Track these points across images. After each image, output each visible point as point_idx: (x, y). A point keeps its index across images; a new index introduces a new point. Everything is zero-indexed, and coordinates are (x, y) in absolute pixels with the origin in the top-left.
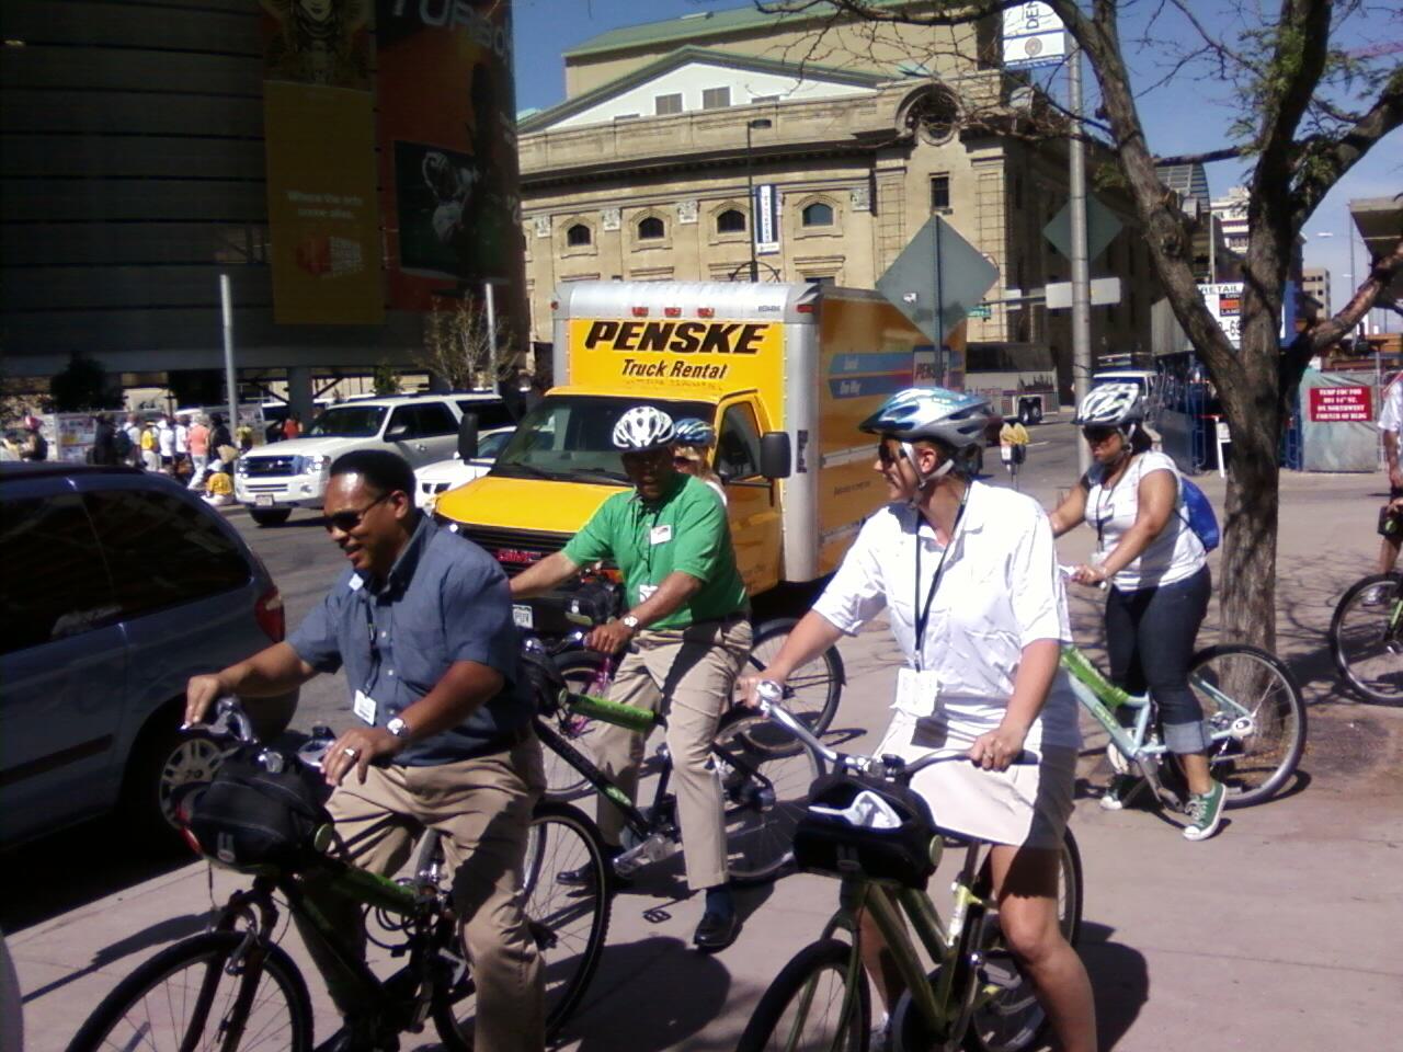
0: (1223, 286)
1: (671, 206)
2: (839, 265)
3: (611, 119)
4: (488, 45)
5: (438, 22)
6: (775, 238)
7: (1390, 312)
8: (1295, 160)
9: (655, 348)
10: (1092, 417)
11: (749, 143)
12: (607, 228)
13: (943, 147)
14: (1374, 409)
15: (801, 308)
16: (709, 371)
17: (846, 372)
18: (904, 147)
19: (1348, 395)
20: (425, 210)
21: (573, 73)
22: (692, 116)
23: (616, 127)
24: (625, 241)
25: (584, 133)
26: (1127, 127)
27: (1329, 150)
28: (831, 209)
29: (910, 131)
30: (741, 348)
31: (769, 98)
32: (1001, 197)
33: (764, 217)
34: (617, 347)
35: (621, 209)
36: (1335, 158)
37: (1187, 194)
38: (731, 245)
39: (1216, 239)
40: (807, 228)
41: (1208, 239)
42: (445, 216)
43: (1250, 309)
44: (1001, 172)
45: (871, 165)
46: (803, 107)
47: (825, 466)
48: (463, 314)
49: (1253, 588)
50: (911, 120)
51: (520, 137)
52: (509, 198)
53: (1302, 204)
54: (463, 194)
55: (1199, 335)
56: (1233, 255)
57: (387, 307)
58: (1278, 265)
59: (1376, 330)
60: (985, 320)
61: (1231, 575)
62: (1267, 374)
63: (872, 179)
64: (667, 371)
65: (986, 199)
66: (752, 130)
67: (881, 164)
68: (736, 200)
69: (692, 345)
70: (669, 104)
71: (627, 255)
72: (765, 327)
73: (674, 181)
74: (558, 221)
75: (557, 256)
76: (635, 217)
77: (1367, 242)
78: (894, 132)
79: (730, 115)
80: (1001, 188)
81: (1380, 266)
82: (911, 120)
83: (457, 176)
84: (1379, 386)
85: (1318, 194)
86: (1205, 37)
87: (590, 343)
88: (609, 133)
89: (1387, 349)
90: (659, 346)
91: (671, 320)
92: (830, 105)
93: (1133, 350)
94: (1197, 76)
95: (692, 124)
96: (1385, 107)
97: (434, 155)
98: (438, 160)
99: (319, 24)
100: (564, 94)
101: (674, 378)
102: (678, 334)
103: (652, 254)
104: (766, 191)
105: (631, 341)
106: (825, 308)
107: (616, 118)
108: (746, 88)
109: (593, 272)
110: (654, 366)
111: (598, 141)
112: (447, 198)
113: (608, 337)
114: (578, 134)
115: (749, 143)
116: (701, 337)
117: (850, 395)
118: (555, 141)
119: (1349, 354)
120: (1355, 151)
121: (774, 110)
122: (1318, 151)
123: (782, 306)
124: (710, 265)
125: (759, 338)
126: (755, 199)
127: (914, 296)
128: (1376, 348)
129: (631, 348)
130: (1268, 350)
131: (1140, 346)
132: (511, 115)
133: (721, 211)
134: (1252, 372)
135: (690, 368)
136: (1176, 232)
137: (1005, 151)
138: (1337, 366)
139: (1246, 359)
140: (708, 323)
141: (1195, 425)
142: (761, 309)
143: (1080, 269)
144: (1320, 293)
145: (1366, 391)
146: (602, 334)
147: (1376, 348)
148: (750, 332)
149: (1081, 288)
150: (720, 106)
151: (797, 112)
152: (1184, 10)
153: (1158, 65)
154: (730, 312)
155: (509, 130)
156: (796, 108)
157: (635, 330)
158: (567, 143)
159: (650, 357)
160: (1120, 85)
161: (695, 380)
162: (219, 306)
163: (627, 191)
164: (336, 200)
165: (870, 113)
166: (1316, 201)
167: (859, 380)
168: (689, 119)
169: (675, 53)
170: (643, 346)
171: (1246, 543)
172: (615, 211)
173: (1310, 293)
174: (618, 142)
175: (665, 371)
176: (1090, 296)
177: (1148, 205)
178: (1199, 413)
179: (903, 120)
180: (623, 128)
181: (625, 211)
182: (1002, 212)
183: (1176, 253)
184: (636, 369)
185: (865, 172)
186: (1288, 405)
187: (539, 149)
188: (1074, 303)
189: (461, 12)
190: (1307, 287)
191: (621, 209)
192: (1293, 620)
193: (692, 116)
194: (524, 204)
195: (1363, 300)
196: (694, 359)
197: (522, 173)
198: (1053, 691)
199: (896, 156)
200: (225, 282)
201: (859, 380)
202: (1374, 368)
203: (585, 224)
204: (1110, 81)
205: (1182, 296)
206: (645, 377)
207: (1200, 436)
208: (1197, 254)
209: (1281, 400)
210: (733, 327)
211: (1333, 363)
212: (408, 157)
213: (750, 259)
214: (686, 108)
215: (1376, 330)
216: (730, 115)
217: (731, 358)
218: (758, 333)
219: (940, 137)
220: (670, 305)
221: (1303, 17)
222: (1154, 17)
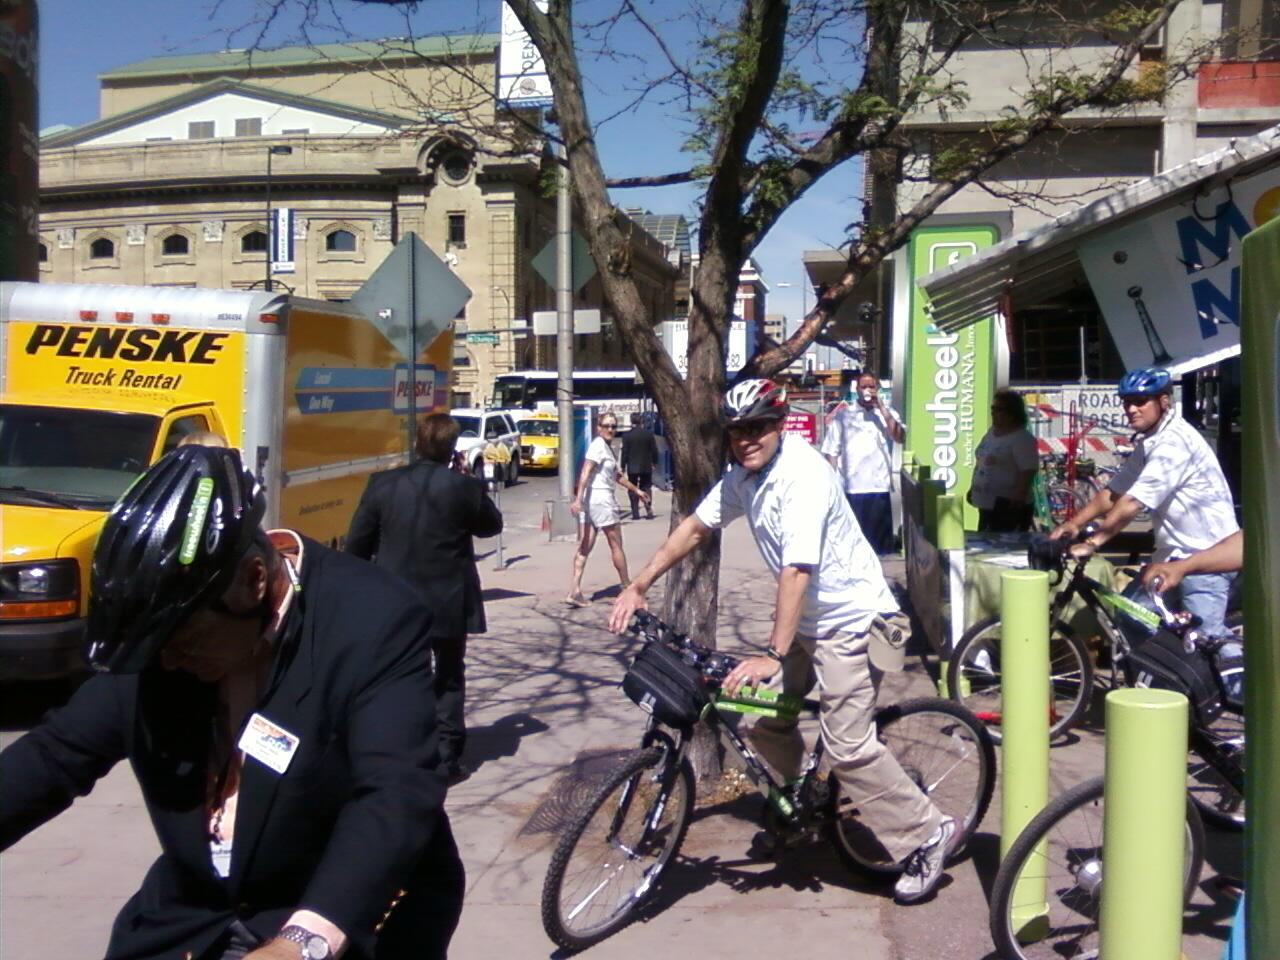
1: (50, 233)
4: (10, 55)
6: (291, 258)
7: (834, 350)
8: (748, 180)
9: (104, 355)
11: (269, 170)
12: (131, 243)
13: (460, 188)
14: (818, 434)
15: (265, 318)
16: (162, 381)
17: (319, 386)
18: (426, 184)
19: (797, 422)
21: (107, 94)
23: (145, 148)
25: (113, 152)
26: (577, 132)
27: (782, 174)
29: (430, 171)
30: (198, 357)
31: (299, 131)
32: (512, 237)
33: (280, 242)
34: (60, 353)
35: (147, 225)
36: (787, 182)
37: (672, 246)
38: (255, 264)
43: (697, 334)
44: (512, 215)
45: (393, 198)
46: (331, 142)
47: (289, 485)
49: (694, 623)
50: (431, 160)
52: (24, 208)
53: (751, 228)
55: (644, 359)
58: (726, 289)
59: (822, 367)
60: (495, 345)
61: (673, 609)
63: (394, 213)
64: (115, 381)
65: (498, 238)
66: (273, 156)
67: (402, 199)
68: (107, 229)
70: (202, 130)
72: (225, 336)
74: (154, 230)
75: (78, 268)
78: (415, 170)
80: (512, 228)
81: (826, 296)
82: (431, 160)
84: (823, 414)
85: (770, 218)
86: (672, 63)
87: (32, 348)
90: (108, 353)
94: (661, 100)
95: (222, 149)
96: (837, 134)
100: (98, 113)
101: (124, 387)
102: (129, 341)
103: (175, 268)
105: (77, 347)
106: (298, 326)
107: (149, 140)
108: (278, 120)
110: (102, 375)
111: (128, 160)
113: (52, 342)
114: (107, 153)
115: (269, 170)
116: (155, 344)
118: (84, 157)
119: (799, 387)
121: (302, 142)
122: (773, 175)
123: (244, 315)
124: (233, 283)
125: (218, 348)
126: (272, 223)
127: (389, 312)
128: (820, 382)
129: (77, 354)
130: (715, 376)
132: (34, 126)
133: (248, 231)
135: (142, 377)
136: (623, 248)
137: (516, 196)
139: (693, 385)
140: (162, 330)
142: (221, 317)
143: (564, 299)
144: (778, 335)
145: (812, 418)
148: (208, 342)
149: (565, 317)
150: (252, 134)
152: (654, 34)
153: (626, 89)
154: (186, 319)
155: (30, 142)
157: (82, 335)
158: (96, 160)
159: (98, 364)
160: (572, 86)
161: (146, 389)
163: (153, 209)
165: (394, 152)
167: (331, 395)
168: (220, 145)
169: (209, 84)
170: (90, 353)
171: (687, 576)
173: (769, 335)
175: (113, 380)
176: (573, 325)
180: (155, 149)
181: (150, 227)
182: (512, 250)
183: (622, 271)
184: (81, 377)
185: (388, 205)
187: (67, 165)
190: (767, 330)
192: (740, 637)
193: (223, 142)
194: (43, 217)
196: (147, 367)
199: (417, 193)
201: (331, 395)
204: (561, 81)
205: (628, 316)
206: (91, 386)
208: (679, 298)
210: (190, 336)
213: (264, 278)
214: (218, 134)
215: (822, 367)
217: (187, 369)
218: (216, 342)
219: (457, 179)
220: (122, 310)
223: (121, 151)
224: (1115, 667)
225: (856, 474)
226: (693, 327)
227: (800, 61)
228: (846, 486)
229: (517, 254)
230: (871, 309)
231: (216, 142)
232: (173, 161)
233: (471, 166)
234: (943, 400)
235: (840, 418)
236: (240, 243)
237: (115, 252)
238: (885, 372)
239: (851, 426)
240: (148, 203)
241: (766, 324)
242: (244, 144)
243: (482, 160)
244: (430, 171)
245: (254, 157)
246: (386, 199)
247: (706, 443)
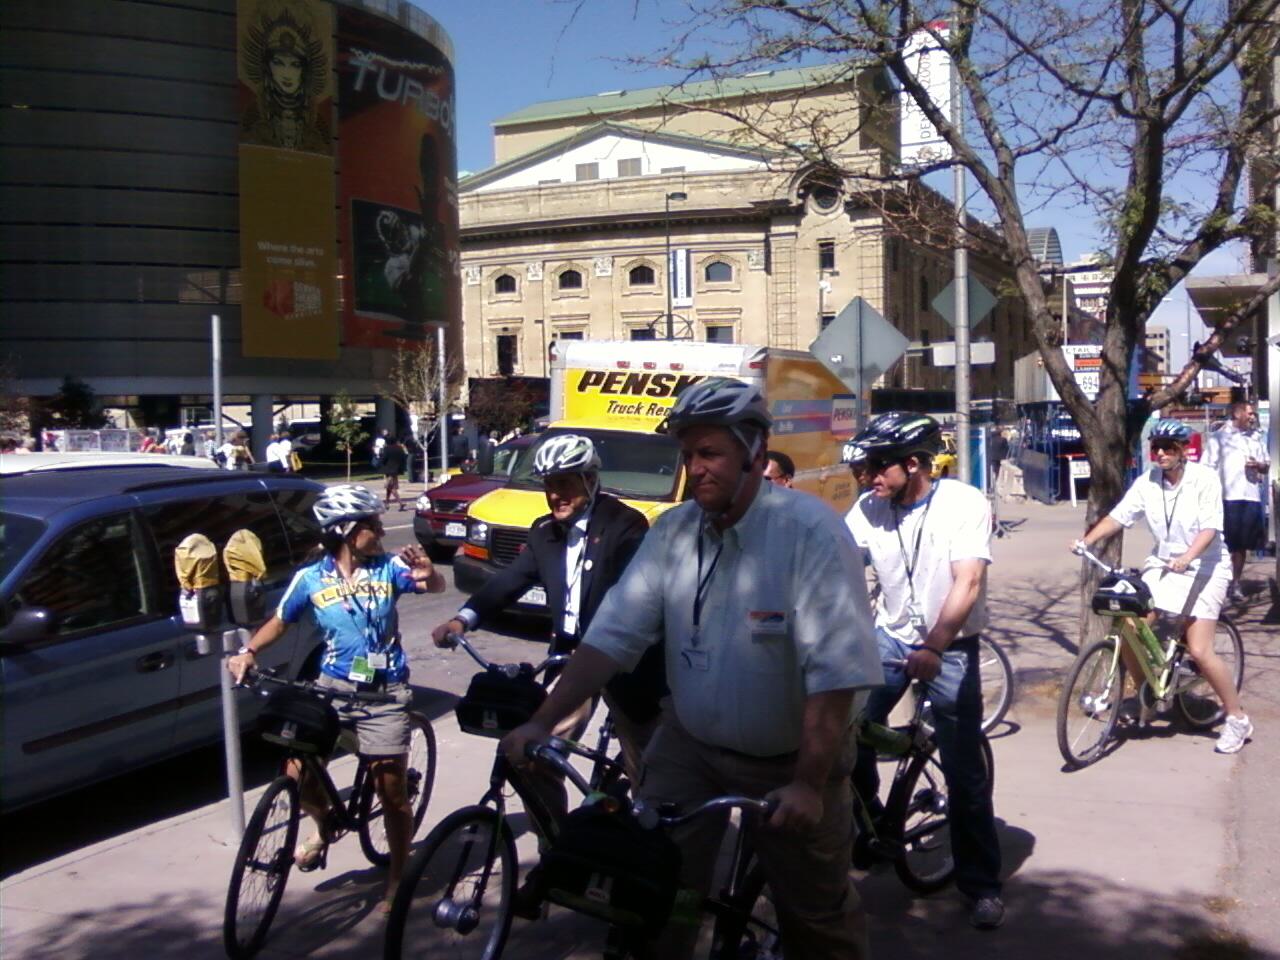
0: (1077, 347)
1: (588, 261)
3: (536, 184)
4: (435, 118)
5: (392, 97)
6: (689, 294)
9: (634, 392)
10: (557, 465)
15: (753, 365)
18: (796, 214)
21: (500, 139)
22: (609, 183)
23: (540, 190)
24: (486, 293)
27: (1163, 271)
28: (730, 267)
29: (800, 201)
35: (544, 262)
39: (1068, 299)
40: (710, 283)
41: (1061, 300)
42: (396, 266)
43: (1106, 382)
45: (766, 230)
46: (707, 178)
48: (423, 354)
50: (801, 191)
51: (460, 195)
52: (450, 252)
54: (412, 247)
56: (1083, 314)
57: (341, 345)
62: (1116, 427)
63: (767, 242)
64: (643, 411)
65: (867, 263)
66: (670, 201)
67: (775, 229)
69: (665, 391)
70: (587, 171)
71: (548, 302)
73: (593, 239)
74: (486, 271)
75: (485, 302)
76: (555, 272)
77: (1200, 312)
78: (787, 201)
79: (642, 183)
81: (1199, 352)
83: (406, 233)
86: (1073, 176)
87: (582, 388)
88: (534, 195)
89: (1217, 400)
90: (637, 391)
91: (648, 372)
92: (730, 177)
93: (994, 396)
95: (608, 189)
96: (1201, 241)
97: (388, 213)
98: (390, 217)
99: (289, 96)
102: (654, 382)
104: (681, 254)
105: (615, 387)
107: (541, 182)
108: (658, 158)
109: (517, 316)
112: (397, 252)
113: (597, 382)
114: (506, 196)
117: (786, 432)
118: (486, 201)
120: (1181, 272)
121: (681, 179)
127: (839, 358)
128: (1208, 399)
129: (615, 392)
131: (999, 392)
133: (635, 265)
134: (1107, 426)
138: (1174, 415)
141: (1052, 462)
144: (1161, 348)
146: (591, 381)
147: (1208, 399)
149: (963, 351)
151: (701, 182)
155: (451, 192)
156: (701, 179)
157: (618, 378)
159: (630, 399)
160: (1017, 225)
162: (209, 341)
163: (549, 247)
164: (300, 250)
166: (1154, 307)
167: (792, 420)
168: (605, 186)
169: (596, 125)
170: (624, 391)
172: (539, 264)
173: (1152, 348)
174: (542, 203)
176: (970, 357)
177: (1035, 308)
178: (1055, 453)
179: (795, 192)
181: (547, 264)
182: (881, 274)
185: (761, 236)
186: (1131, 449)
187: (472, 208)
188: (957, 362)
189: (412, 88)
190: (1149, 343)
191: (544, 262)
193: (609, 183)
194: (464, 255)
195: (1187, 376)
197: (461, 228)
200: (215, 321)
201: (792, 420)
202: (1204, 417)
203: (510, 274)
206: (625, 415)
207: (1056, 472)
209: (1127, 446)
211: (1170, 412)
212: (365, 214)
216: (642, 183)
219: (827, 207)
221: (1144, 185)
222: (1040, 173)
223: (518, 194)
224: (1044, 346)
225: (1232, 485)
226: (1103, 376)
227: (1173, 188)
228: (1225, 493)
229: (885, 277)
230: (1248, 342)
231: (603, 183)
232: (566, 201)
233: (840, 194)
235: (1219, 437)
236: (627, 276)
237: (517, 287)
238: (1264, 396)
239: (1227, 444)
240: (545, 242)
241: (1147, 336)
242: (628, 184)
243: (849, 187)
244: (800, 201)
245: (637, 195)
246: (759, 231)
247: (1113, 456)
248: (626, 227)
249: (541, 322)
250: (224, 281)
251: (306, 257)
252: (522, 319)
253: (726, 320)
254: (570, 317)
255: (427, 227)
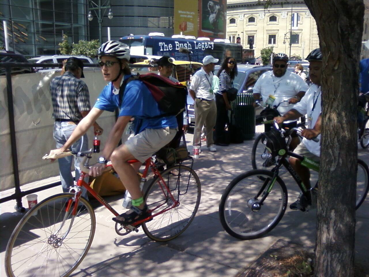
1: (257, 14)
2: (255, 32)
20: (208, 16)
24: (245, 23)
35: (288, 12)
42: (212, 17)
68: (275, 13)
71: (245, 26)
112: (212, 13)
124: (267, 30)
164: (189, 13)
181: (245, 15)
198: (93, 245)
203: (253, 17)
234: (182, 45)
237: (236, 22)
248: (254, 5)
249: (243, 32)
250: (159, 21)
251: (190, 15)
252: (279, 30)
253: (253, 34)
254: (251, 31)
255: (220, 6)
